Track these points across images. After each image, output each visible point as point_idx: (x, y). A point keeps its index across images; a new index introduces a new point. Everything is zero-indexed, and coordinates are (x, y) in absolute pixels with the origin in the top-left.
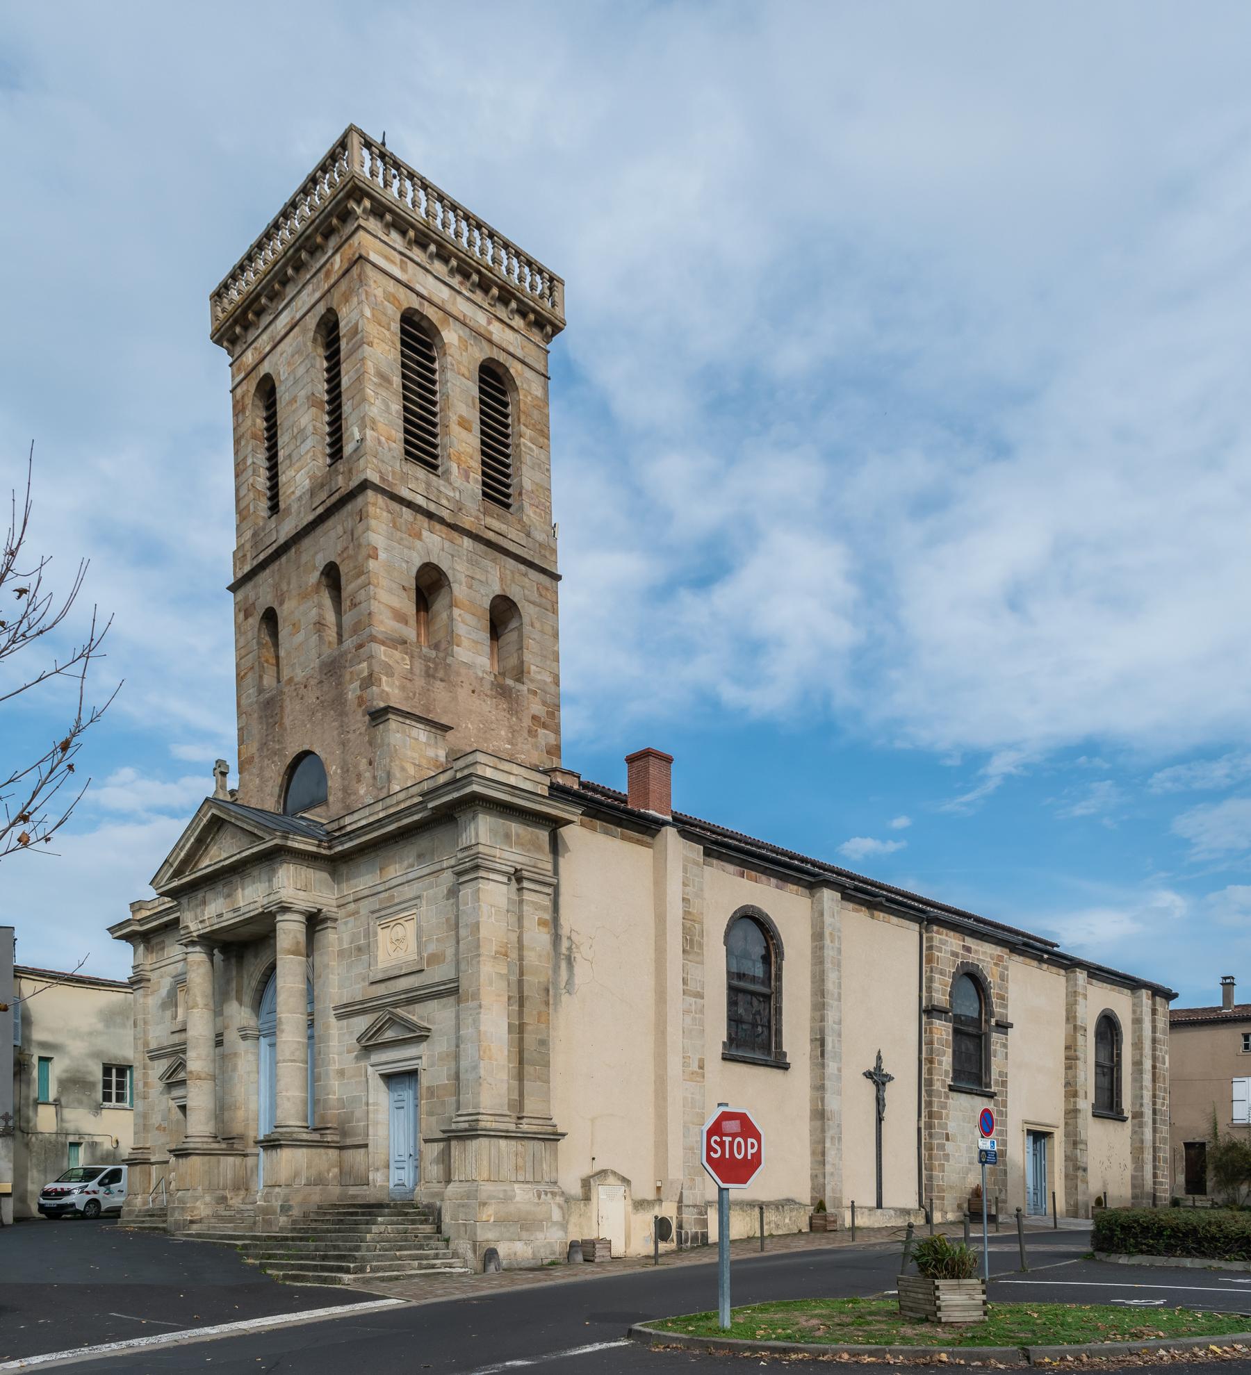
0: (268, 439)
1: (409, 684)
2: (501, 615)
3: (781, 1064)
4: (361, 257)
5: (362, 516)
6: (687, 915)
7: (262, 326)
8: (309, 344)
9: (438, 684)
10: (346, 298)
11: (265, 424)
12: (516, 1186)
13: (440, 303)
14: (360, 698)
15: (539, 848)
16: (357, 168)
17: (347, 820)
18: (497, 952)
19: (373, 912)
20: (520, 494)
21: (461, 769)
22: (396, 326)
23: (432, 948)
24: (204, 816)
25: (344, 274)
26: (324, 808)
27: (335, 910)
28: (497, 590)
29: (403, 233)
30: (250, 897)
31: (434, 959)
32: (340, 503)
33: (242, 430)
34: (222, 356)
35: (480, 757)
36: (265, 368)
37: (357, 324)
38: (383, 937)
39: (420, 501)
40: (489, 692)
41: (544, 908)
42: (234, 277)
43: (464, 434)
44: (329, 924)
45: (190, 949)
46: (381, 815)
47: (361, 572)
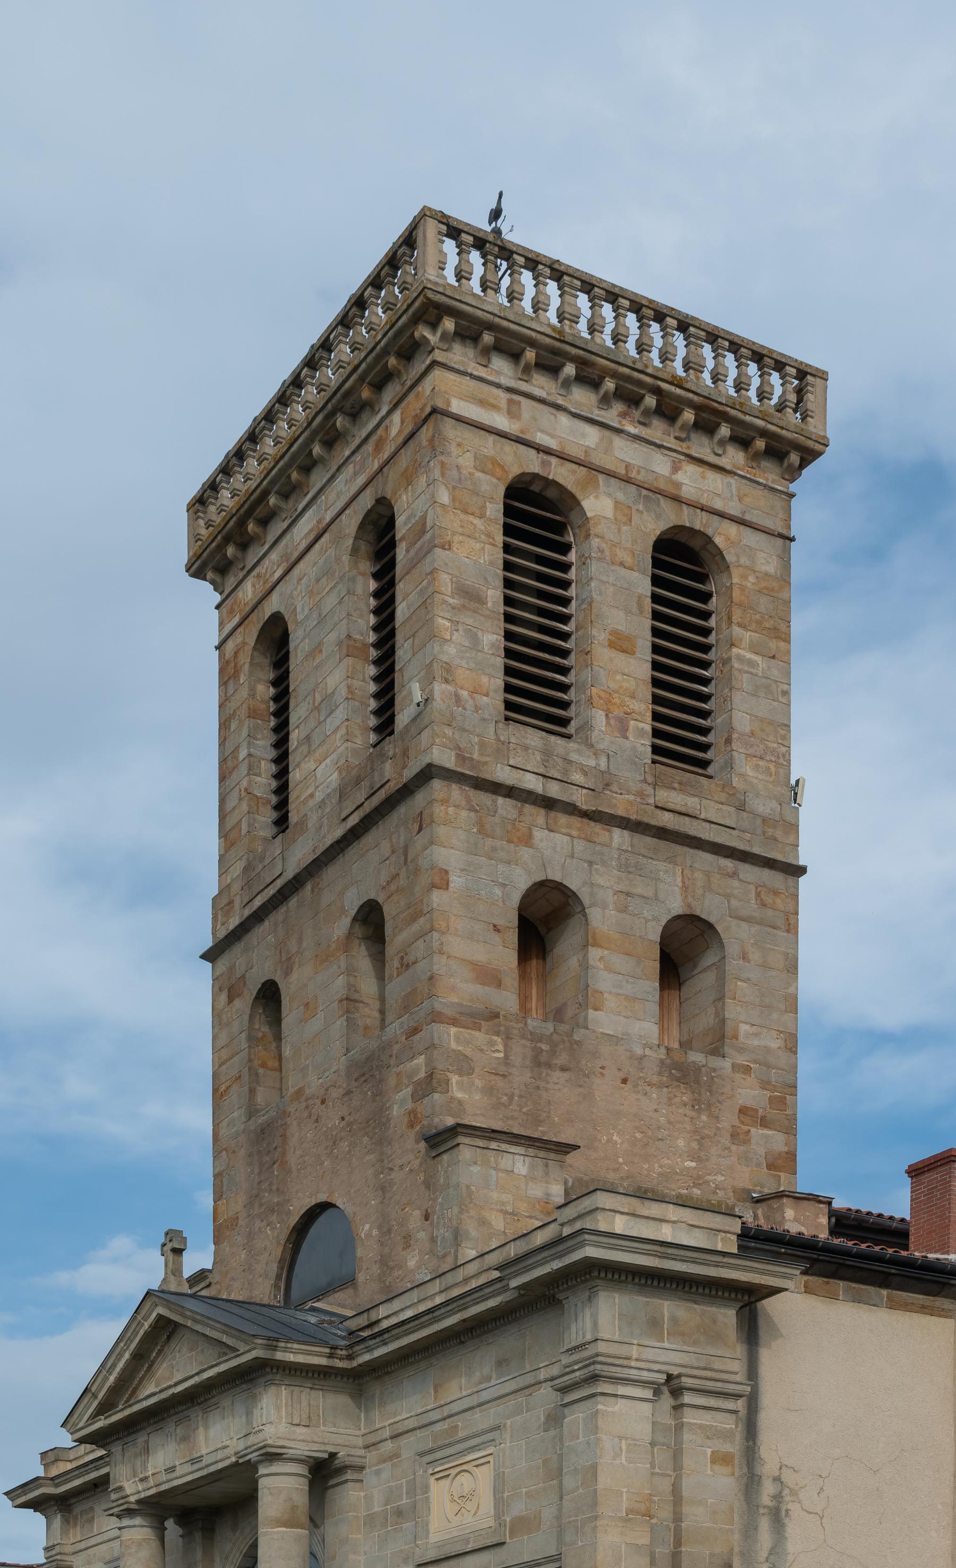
0: (276, 714)
1: (500, 1083)
2: (682, 952)
4: (434, 411)
5: (422, 822)
7: (270, 539)
8: (346, 558)
9: (557, 1076)
10: (408, 479)
11: (272, 691)
14: (412, 1114)
15: (716, 1338)
16: (431, 274)
17: (383, 1311)
19: (422, 1454)
20: (728, 741)
21: (571, 1222)
22: (495, 510)
23: (518, 1508)
24: (145, 1318)
25: (405, 443)
26: (350, 1291)
27: (361, 1452)
28: (676, 906)
29: (516, 357)
30: (217, 1440)
31: (522, 1525)
32: (385, 806)
33: (232, 706)
34: (205, 594)
35: (603, 1200)
36: (273, 605)
37: (424, 518)
38: (439, 1492)
39: (532, 783)
40: (655, 1079)
41: (726, 1436)
42: (225, 470)
43: (620, 660)
44: (349, 1475)
45: (126, 1522)
46: (438, 1300)
47: (417, 912)
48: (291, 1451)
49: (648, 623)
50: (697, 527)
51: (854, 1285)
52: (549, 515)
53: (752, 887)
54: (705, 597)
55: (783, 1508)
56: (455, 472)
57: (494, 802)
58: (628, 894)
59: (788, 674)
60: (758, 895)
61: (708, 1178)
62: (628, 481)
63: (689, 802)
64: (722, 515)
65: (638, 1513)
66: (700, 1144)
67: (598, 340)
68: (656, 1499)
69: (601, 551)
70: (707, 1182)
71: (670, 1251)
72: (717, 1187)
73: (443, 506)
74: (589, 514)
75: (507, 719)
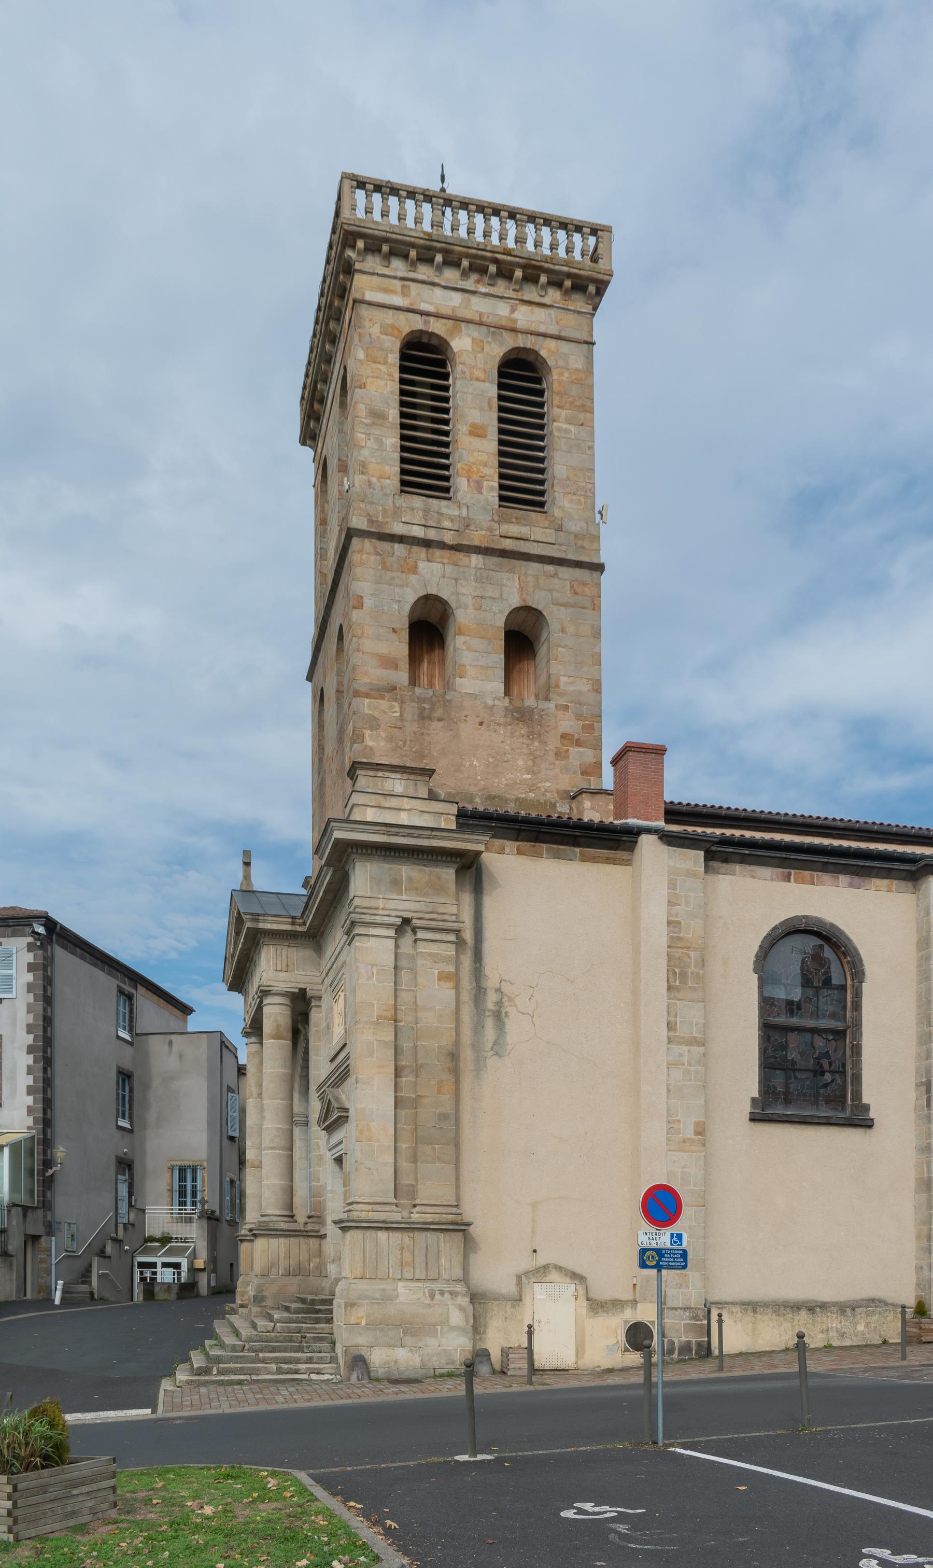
3: (861, 1120)
6: (674, 942)
9: (436, 725)
12: (400, 1284)
13: (450, 313)
15: (440, 889)
18: (379, 1017)
22: (394, 358)
28: (515, 601)
29: (406, 257)
39: (418, 532)
40: (502, 720)
41: (446, 959)
43: (477, 442)
48: (275, 989)
49: (495, 415)
50: (528, 346)
51: (554, 846)
52: (434, 356)
53: (568, 583)
54: (541, 393)
55: (503, 1011)
56: (368, 338)
57: (393, 547)
58: (482, 597)
59: (593, 434)
60: (572, 587)
61: (540, 785)
62: (481, 324)
63: (523, 530)
64: (545, 335)
65: (386, 1018)
66: (534, 762)
67: (539, 252)
68: (403, 1008)
69: (463, 372)
70: (539, 788)
71: (393, 830)
72: (546, 791)
73: (360, 361)
74: (455, 350)
75: (402, 491)
